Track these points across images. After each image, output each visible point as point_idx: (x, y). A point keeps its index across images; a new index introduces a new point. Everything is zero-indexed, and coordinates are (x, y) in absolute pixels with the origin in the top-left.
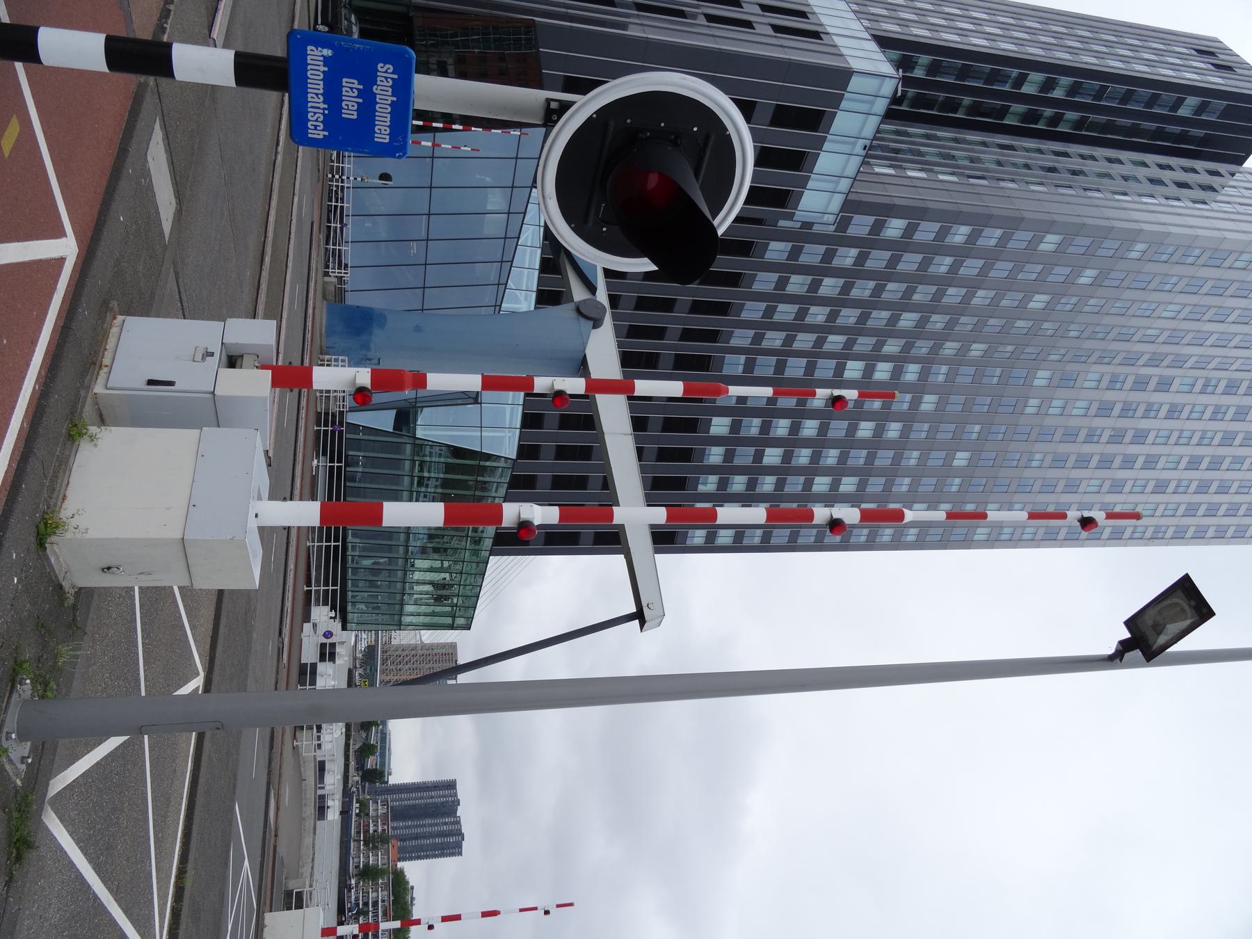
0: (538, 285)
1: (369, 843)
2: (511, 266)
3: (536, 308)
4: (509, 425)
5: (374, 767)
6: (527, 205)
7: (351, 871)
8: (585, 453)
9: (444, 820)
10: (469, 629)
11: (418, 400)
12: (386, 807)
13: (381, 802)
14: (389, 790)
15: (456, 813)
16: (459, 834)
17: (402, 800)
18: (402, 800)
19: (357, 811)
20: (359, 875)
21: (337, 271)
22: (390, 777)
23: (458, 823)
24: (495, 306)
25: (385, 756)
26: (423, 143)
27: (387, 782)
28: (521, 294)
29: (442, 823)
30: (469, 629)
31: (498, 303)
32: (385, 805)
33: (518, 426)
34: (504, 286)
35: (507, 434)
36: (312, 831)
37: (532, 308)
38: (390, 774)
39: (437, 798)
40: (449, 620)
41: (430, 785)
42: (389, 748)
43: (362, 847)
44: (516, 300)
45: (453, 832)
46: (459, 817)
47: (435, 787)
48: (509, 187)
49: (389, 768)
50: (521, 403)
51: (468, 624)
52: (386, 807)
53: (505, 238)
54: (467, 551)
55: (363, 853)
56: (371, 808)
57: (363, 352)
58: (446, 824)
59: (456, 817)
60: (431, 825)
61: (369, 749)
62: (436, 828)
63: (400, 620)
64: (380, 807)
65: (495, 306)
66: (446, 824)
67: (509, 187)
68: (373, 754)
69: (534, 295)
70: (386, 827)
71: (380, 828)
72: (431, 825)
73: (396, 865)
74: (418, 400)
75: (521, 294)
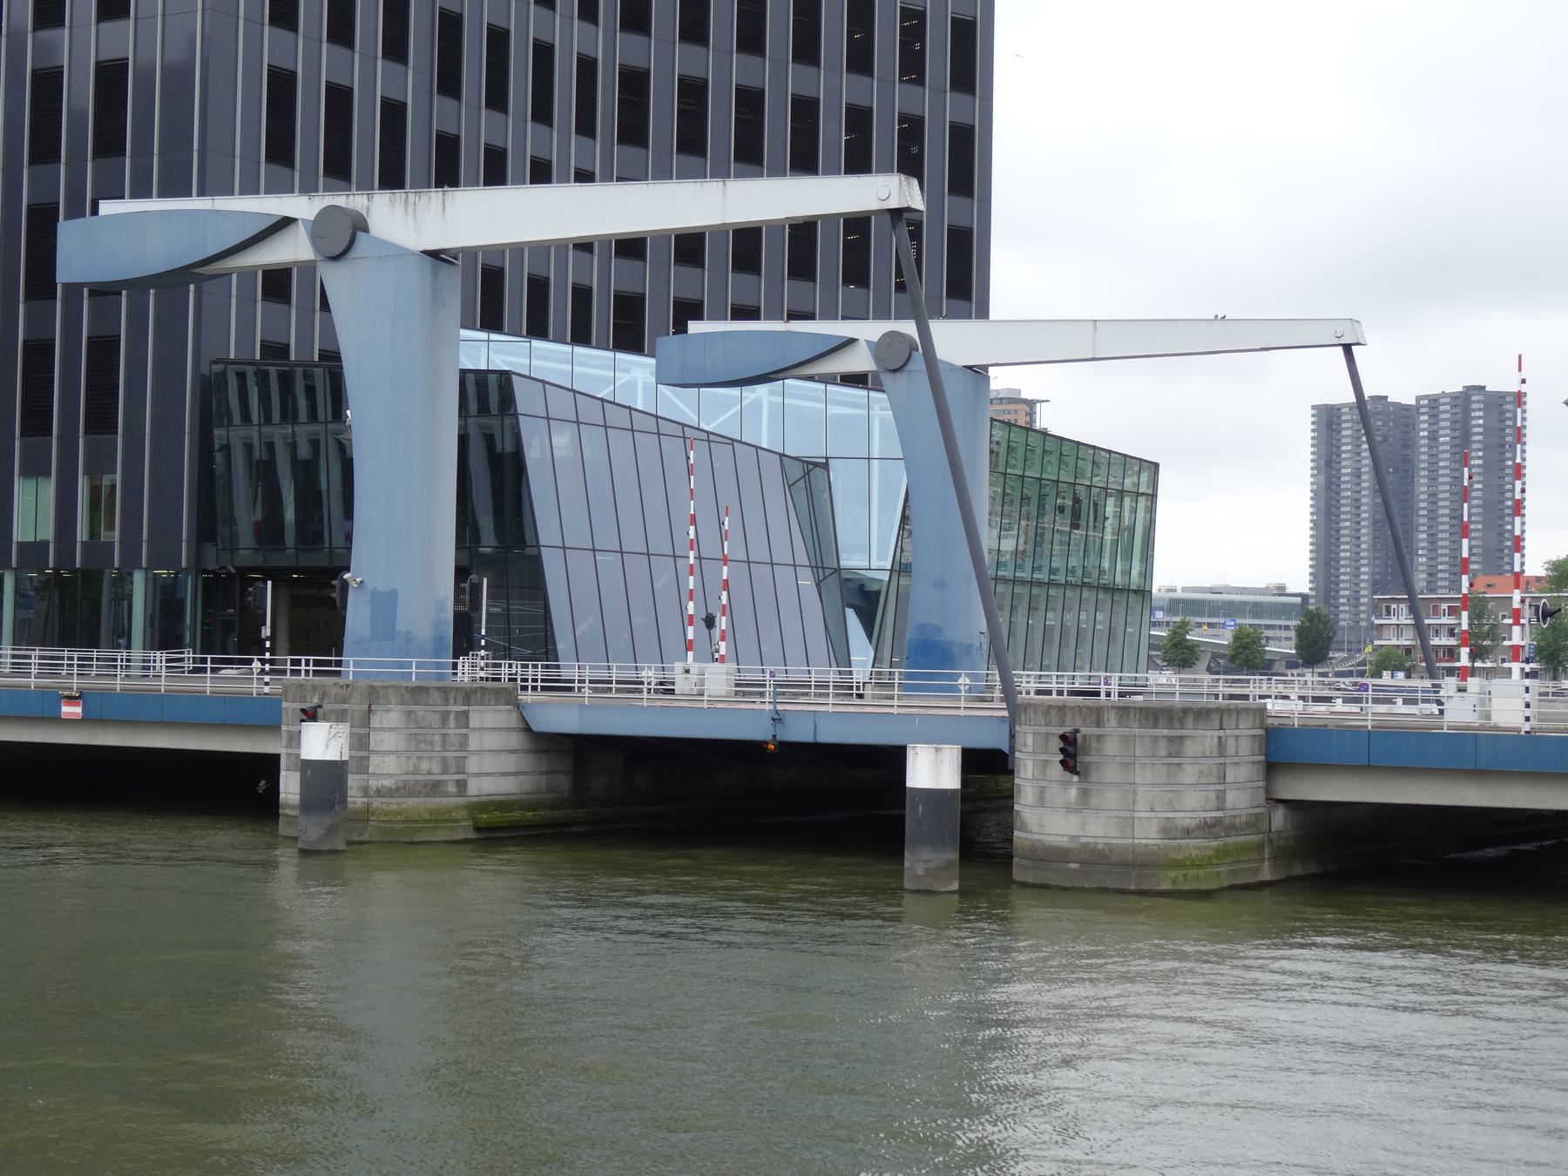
0: (565, 343)
1: (1481, 646)
2: (614, 403)
3: (652, 355)
4: (864, 409)
5: (1292, 634)
6: (617, 404)
7: (1241, 839)
8: (633, 132)
9: (1424, 442)
10: (1156, 465)
11: (814, 565)
12: (1394, 606)
13: (1380, 616)
14: (1327, 592)
15: (1407, 408)
16: (1465, 398)
17: (1356, 558)
18: (1356, 558)
19: (1401, 675)
20: (1555, 670)
21: (768, 688)
22: (1289, 590)
23: (1434, 401)
24: (709, 441)
25: (1230, 604)
26: (691, 578)
27: (1305, 597)
28: (619, 379)
29: (1430, 448)
30: (1156, 465)
31: (704, 436)
32: (1388, 609)
33: (864, 393)
34: (710, 435)
35: (1047, 577)
36: (1553, 704)
37: (652, 361)
38: (1281, 590)
39: (1356, 461)
40: (1142, 502)
41: (1322, 479)
42: (1212, 591)
43: (1489, 665)
44: (632, 385)
45: (1459, 417)
46: (1418, 398)
47: (1329, 464)
48: (549, 422)
49: (1265, 591)
50: (822, 386)
51: (1149, 468)
52: (1394, 606)
53: (578, 423)
54: (1027, 474)
55: (1503, 661)
56: (1394, 642)
57: (974, 652)
58: (1433, 437)
59: (1418, 407)
60: (1433, 479)
61: (1245, 647)
62: (1442, 464)
63: (1135, 592)
64: (1394, 621)
65: (709, 441)
66: (1433, 437)
67: (549, 422)
68: (1256, 640)
69: (621, 356)
70: (1444, 606)
71: (1444, 620)
72: (1433, 479)
73: (1538, 579)
74: (814, 565)
75: (619, 379)
